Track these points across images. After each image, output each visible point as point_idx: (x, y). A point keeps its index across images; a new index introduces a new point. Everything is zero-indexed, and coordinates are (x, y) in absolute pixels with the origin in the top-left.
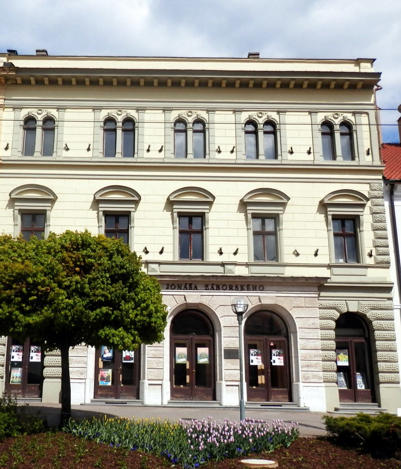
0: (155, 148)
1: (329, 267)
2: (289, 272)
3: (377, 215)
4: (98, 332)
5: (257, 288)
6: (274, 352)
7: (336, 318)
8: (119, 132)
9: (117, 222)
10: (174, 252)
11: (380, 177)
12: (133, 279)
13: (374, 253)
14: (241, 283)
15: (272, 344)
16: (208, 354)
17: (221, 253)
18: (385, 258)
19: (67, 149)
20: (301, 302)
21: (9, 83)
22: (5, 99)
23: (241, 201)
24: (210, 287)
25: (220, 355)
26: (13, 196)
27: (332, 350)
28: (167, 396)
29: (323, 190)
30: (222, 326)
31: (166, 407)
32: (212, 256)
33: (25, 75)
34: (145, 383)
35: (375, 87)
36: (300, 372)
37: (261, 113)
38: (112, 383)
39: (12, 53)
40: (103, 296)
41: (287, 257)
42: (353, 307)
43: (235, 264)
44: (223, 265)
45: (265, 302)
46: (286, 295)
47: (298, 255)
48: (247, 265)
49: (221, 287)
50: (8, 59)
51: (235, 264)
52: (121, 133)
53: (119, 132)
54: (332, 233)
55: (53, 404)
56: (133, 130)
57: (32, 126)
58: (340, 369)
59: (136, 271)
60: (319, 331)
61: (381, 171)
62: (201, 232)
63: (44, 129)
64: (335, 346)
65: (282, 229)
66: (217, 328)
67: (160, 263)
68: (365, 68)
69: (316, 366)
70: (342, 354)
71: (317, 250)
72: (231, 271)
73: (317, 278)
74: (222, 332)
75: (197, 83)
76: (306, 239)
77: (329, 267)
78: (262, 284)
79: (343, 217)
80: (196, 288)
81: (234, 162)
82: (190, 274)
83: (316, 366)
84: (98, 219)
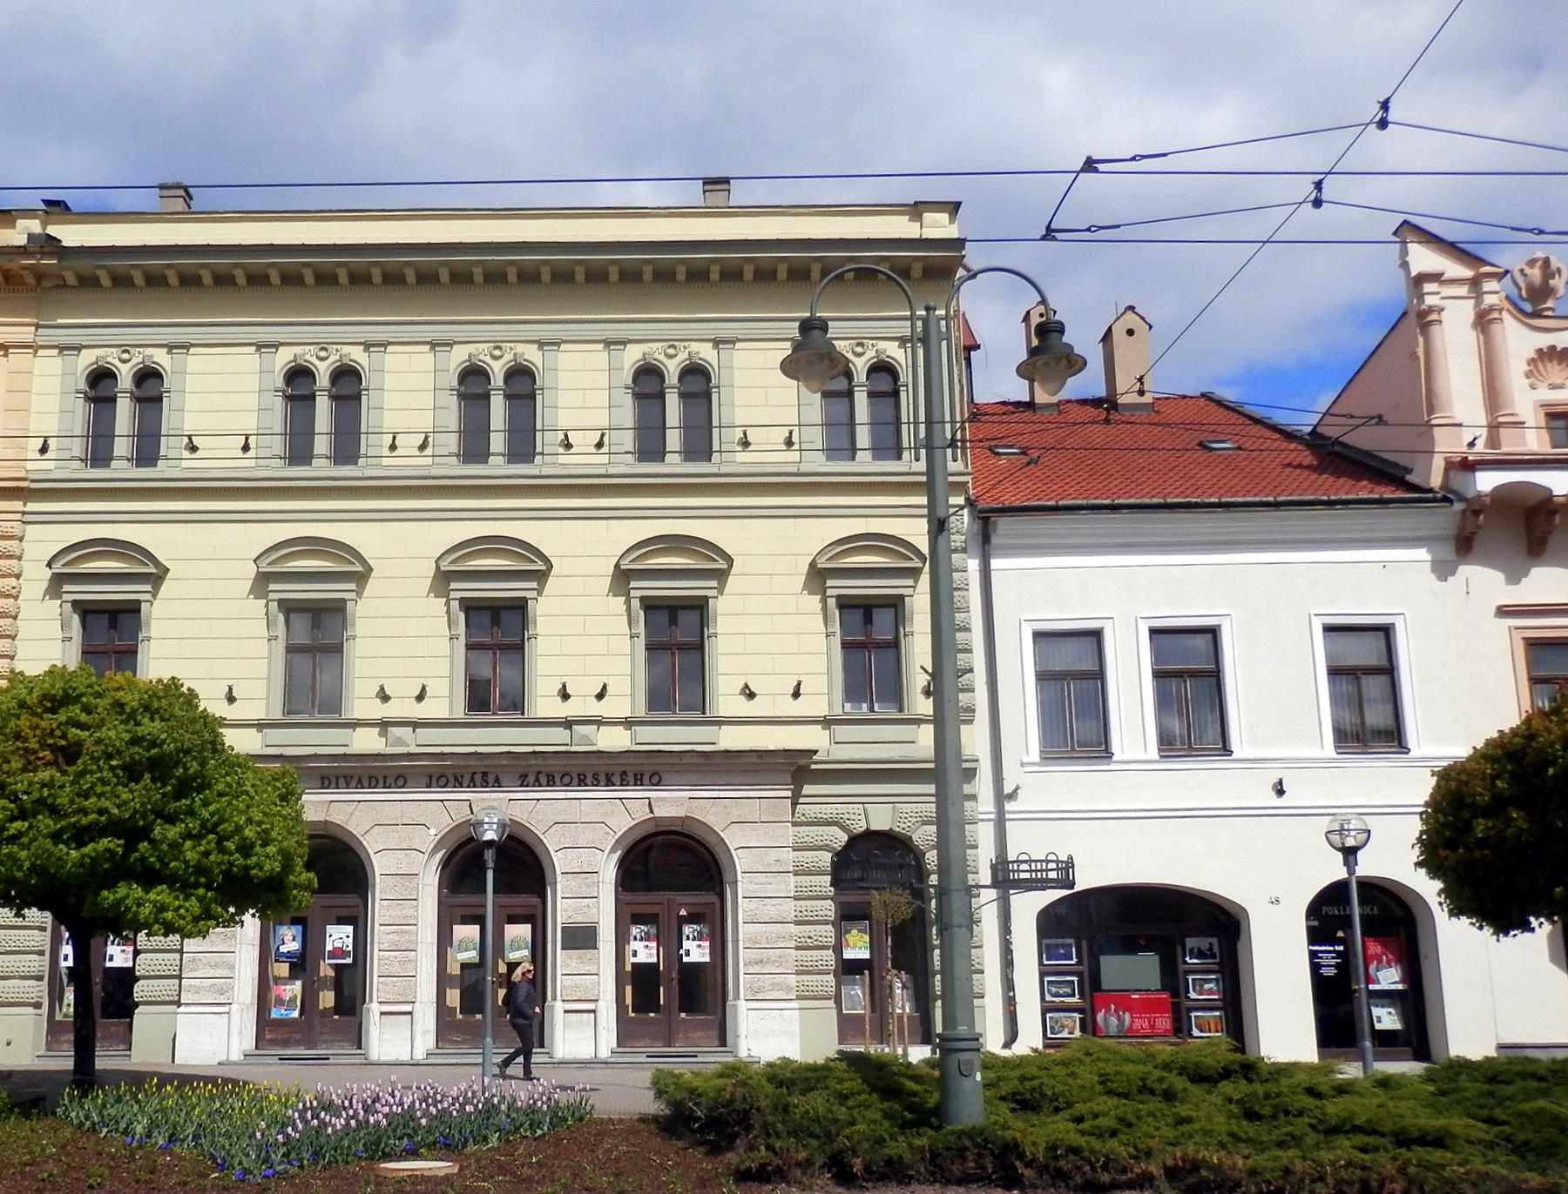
1: (827, 722)
2: (731, 739)
4: (98, 894)
5: (646, 779)
6: (687, 930)
7: (838, 846)
8: (861, 398)
9: (673, 621)
10: (451, 697)
12: (186, 769)
14: (606, 769)
15: (683, 912)
16: (529, 939)
17: (565, 696)
20: (750, 810)
21: (46, 284)
22: (38, 326)
24: (531, 779)
25: (554, 941)
26: (58, 568)
27: (826, 923)
28: (426, 1040)
29: (814, 535)
30: (558, 872)
32: (543, 703)
33: (84, 265)
34: (373, 1009)
35: (961, 272)
36: (742, 976)
37: (674, 347)
38: (301, 1014)
39: (56, 208)
40: (101, 812)
41: (725, 701)
42: (881, 819)
43: (599, 722)
44: (568, 724)
45: (662, 811)
46: (715, 794)
47: (751, 695)
48: (628, 723)
49: (557, 779)
50: (44, 225)
51: (599, 722)
52: (324, 407)
53: (861, 398)
54: (837, 642)
55: (159, 1065)
56: (707, 395)
57: (154, 393)
58: (849, 969)
59: (216, 745)
60: (792, 879)
62: (698, 648)
63: (138, 400)
64: (832, 914)
65: (716, 635)
66: (727, 877)
67: (415, 725)
68: (938, 226)
69: (780, 961)
70: (855, 932)
71: (799, 684)
72: (586, 740)
73: (786, 752)
74: (559, 886)
75: (748, 273)
76: (773, 657)
77: (827, 722)
78: (655, 768)
79: (672, 603)
80: (498, 783)
81: (795, 470)
82: (513, 749)
83: (780, 961)
84: (629, 615)
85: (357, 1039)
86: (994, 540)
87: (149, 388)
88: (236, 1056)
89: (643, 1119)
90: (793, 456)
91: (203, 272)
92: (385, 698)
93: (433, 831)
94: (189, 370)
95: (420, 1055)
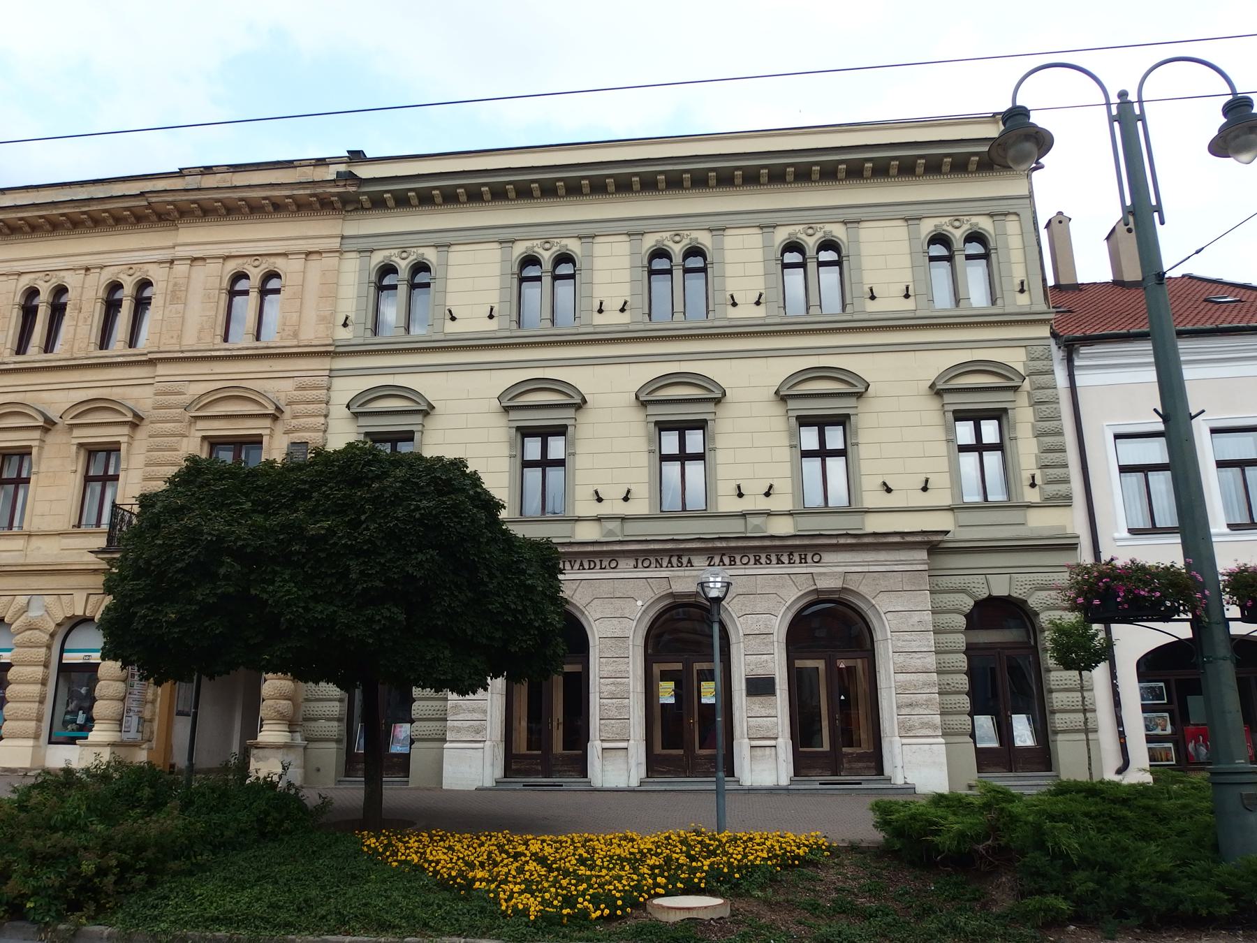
0: (613, 304)
2: (875, 524)
3: (1043, 407)
7: (967, 610)
11: (1045, 331)
13: (1038, 481)
18: (1062, 488)
19: (873, 298)
23: (932, 386)
31: (634, 791)
34: (595, 747)
44: (743, 515)
45: (823, 584)
61: (1049, 320)
64: (965, 665)
65: (857, 444)
67: (623, 519)
69: (927, 704)
85: (580, 766)
86: (1077, 363)
87: (422, 278)
88: (489, 783)
89: (853, 848)
90: (909, 305)
91: (585, 182)
92: (600, 500)
93: (640, 603)
94: (726, 247)
95: (634, 783)
